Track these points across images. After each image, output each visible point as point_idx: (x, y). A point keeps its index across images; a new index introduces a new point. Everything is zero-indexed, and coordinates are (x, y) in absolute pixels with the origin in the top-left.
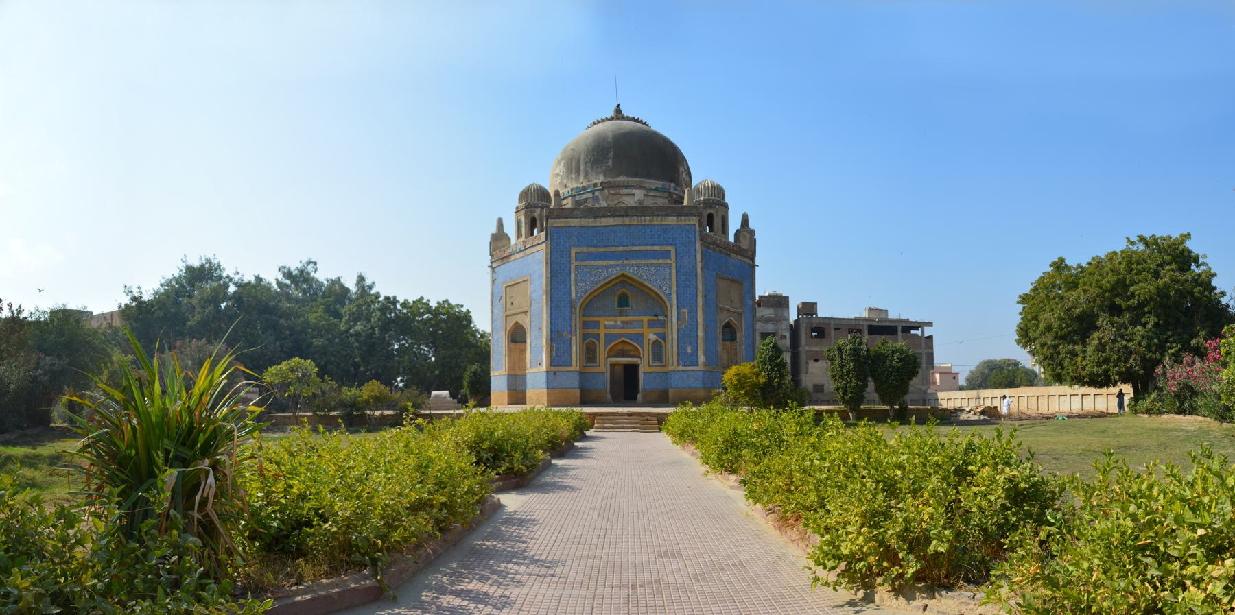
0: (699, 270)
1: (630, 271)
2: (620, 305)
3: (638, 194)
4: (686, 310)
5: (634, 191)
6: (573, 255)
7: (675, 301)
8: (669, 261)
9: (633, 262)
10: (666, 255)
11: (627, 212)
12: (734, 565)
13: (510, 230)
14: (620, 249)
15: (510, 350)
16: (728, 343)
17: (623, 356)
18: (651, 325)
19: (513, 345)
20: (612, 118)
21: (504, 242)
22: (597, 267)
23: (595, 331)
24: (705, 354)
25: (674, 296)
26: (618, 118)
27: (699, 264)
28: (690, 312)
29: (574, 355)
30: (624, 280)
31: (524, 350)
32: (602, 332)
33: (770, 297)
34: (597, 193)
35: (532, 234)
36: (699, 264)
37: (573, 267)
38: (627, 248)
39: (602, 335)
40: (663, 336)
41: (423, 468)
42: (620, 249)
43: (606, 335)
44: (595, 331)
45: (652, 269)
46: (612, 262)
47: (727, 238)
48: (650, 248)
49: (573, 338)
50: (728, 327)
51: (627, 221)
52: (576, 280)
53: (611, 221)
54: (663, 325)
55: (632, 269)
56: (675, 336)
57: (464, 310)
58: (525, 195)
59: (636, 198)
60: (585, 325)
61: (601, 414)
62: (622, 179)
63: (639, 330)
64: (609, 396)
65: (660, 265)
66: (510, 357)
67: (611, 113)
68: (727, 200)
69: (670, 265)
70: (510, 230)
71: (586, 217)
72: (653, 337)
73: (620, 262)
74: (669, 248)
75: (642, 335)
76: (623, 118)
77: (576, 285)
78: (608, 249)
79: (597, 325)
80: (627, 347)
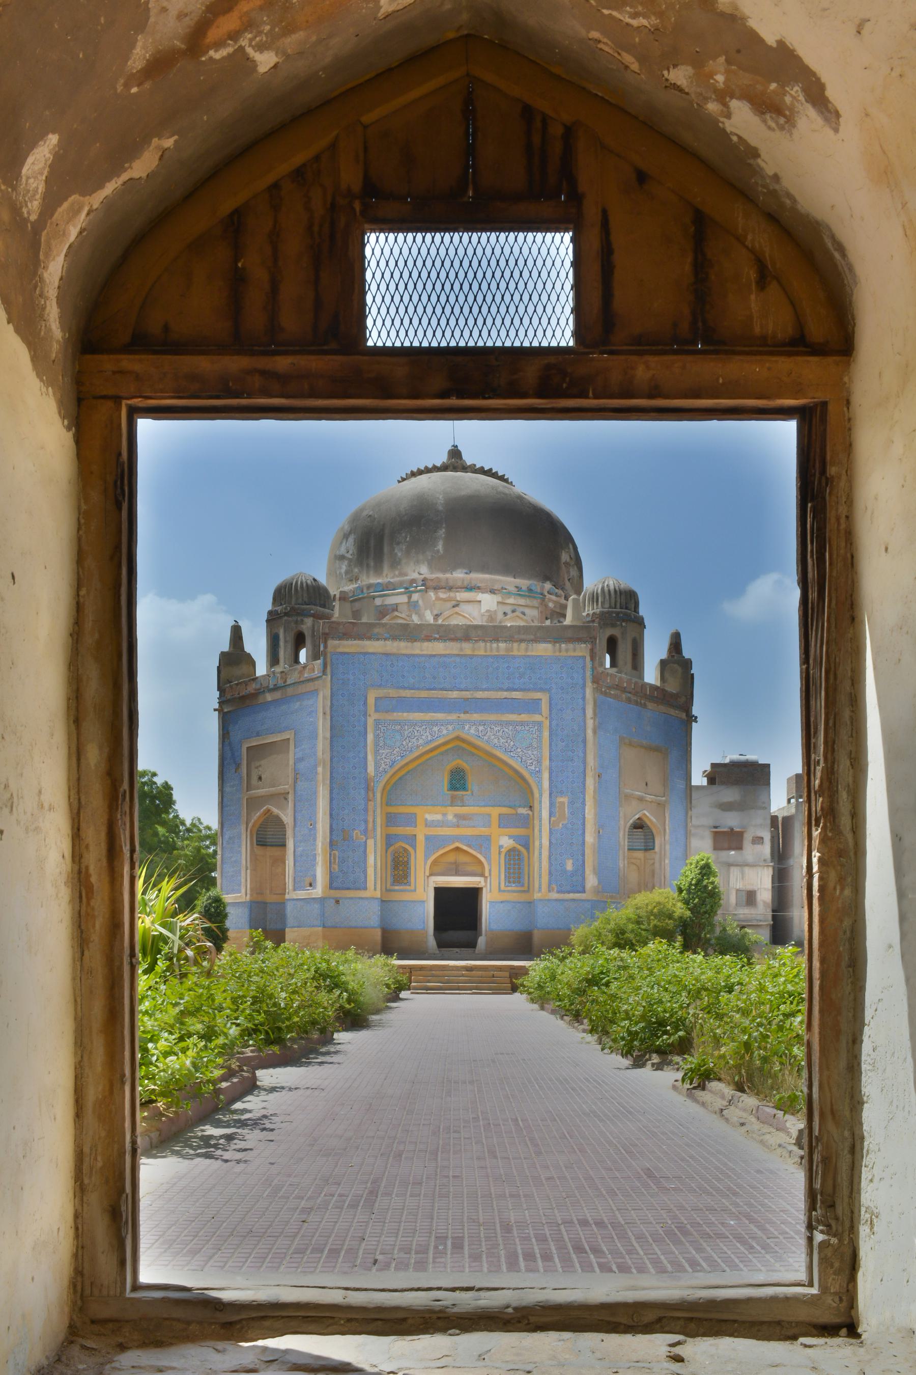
0: (590, 732)
1: (469, 733)
2: (453, 787)
3: (488, 602)
4: (564, 799)
5: (480, 596)
6: (371, 701)
7: (546, 784)
8: (537, 718)
9: (476, 717)
10: (533, 706)
11: (467, 634)
12: (669, 1233)
13: (256, 645)
14: (455, 694)
15: (254, 858)
16: (640, 855)
17: (457, 873)
18: (504, 822)
19: (259, 851)
20: (444, 468)
21: (244, 669)
22: (414, 724)
23: (409, 830)
24: (598, 872)
25: (546, 775)
26: (455, 469)
27: (590, 723)
28: (572, 803)
29: (370, 871)
30: (460, 746)
31: (282, 860)
32: (421, 834)
33: (734, 765)
34: (415, 597)
35: (296, 660)
36: (590, 723)
37: (370, 722)
38: (467, 694)
39: (421, 839)
40: (527, 843)
41: (680, 891)
42: (455, 694)
43: (428, 838)
44: (409, 830)
45: (509, 730)
46: (440, 716)
47: (641, 676)
48: (505, 694)
49: (370, 843)
50: (639, 825)
51: (467, 648)
52: (376, 744)
53: (439, 647)
54: (526, 822)
55: (479, 729)
56: (546, 842)
57: (159, 780)
58: (282, 593)
59: (484, 608)
60: (391, 820)
61: (422, 968)
62: (459, 575)
63: (484, 831)
64: (432, 942)
65: (522, 723)
66: (254, 870)
67: (441, 458)
68: (642, 611)
69: (540, 724)
70: (256, 645)
71: (394, 638)
72: (506, 842)
73: (454, 717)
74: (538, 695)
75: (488, 838)
76: (465, 468)
77: (376, 752)
78: (434, 694)
79: (411, 820)
80: (462, 858)
